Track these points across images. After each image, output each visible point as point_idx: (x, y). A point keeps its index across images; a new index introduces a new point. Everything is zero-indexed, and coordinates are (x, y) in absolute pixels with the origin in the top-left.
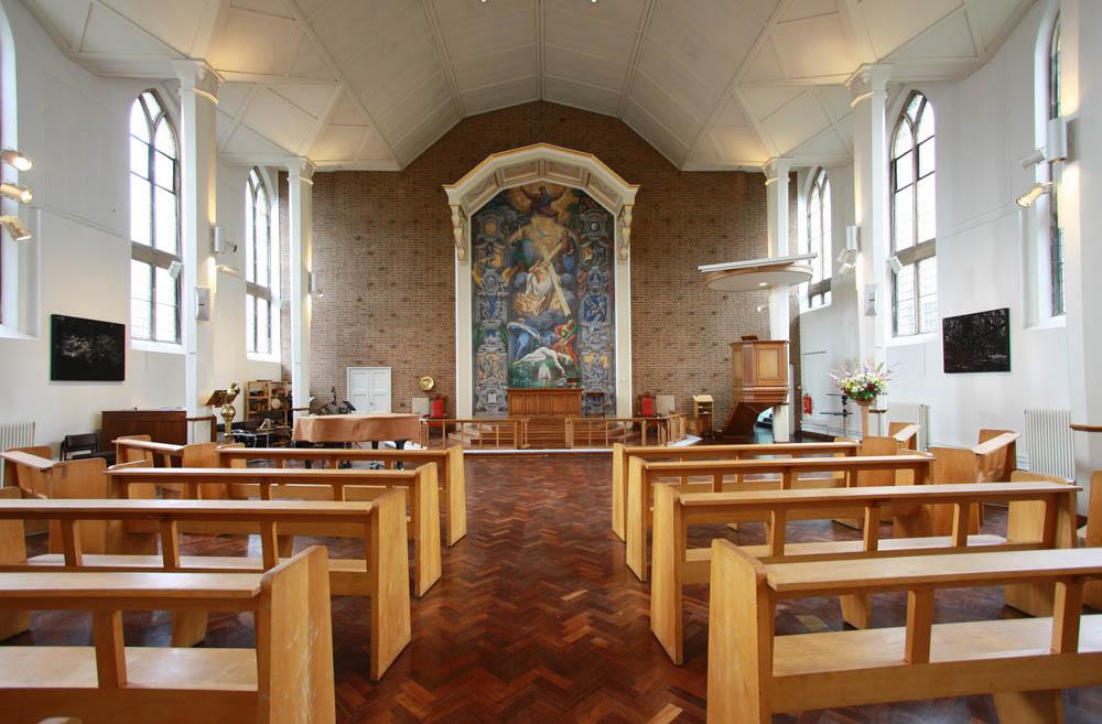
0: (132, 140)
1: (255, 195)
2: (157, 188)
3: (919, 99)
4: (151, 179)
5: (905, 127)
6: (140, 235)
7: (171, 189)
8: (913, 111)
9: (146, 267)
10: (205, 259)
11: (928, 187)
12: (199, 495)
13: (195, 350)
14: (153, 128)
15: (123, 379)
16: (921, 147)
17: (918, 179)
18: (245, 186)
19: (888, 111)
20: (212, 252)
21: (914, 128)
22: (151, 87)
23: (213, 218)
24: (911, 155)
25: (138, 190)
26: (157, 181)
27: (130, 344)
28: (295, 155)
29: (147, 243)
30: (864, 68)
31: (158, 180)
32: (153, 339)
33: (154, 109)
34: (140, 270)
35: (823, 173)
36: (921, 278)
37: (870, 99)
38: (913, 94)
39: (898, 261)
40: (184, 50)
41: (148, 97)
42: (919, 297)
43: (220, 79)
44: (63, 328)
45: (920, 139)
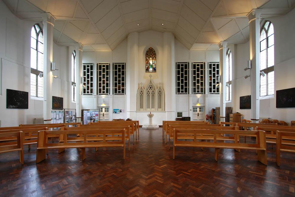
0: (32, 38)
1: (74, 57)
2: (39, 53)
3: (268, 23)
4: (37, 50)
5: (263, 31)
6: (33, 66)
7: (36, 49)
8: (266, 27)
9: (35, 76)
10: (49, 72)
11: (271, 50)
12: (191, 87)
13: (257, 100)
14: (38, 35)
15: (28, 108)
16: (269, 38)
17: (260, 52)
18: (72, 56)
19: (260, 23)
20: (51, 70)
21: (267, 32)
22: (37, 23)
23: (51, 60)
24: (265, 40)
25: (33, 53)
26: (39, 50)
27: (30, 98)
28: (77, 43)
29: (36, 69)
30: (253, 10)
31: (39, 49)
32: (37, 96)
33: (38, 30)
34: (33, 76)
35: (229, 50)
36: (268, 78)
37: (255, 20)
38: (266, 21)
39: (264, 73)
40: (44, 10)
41: (36, 26)
42: (268, 84)
43: (55, 19)
44: (10, 93)
45: (269, 35)
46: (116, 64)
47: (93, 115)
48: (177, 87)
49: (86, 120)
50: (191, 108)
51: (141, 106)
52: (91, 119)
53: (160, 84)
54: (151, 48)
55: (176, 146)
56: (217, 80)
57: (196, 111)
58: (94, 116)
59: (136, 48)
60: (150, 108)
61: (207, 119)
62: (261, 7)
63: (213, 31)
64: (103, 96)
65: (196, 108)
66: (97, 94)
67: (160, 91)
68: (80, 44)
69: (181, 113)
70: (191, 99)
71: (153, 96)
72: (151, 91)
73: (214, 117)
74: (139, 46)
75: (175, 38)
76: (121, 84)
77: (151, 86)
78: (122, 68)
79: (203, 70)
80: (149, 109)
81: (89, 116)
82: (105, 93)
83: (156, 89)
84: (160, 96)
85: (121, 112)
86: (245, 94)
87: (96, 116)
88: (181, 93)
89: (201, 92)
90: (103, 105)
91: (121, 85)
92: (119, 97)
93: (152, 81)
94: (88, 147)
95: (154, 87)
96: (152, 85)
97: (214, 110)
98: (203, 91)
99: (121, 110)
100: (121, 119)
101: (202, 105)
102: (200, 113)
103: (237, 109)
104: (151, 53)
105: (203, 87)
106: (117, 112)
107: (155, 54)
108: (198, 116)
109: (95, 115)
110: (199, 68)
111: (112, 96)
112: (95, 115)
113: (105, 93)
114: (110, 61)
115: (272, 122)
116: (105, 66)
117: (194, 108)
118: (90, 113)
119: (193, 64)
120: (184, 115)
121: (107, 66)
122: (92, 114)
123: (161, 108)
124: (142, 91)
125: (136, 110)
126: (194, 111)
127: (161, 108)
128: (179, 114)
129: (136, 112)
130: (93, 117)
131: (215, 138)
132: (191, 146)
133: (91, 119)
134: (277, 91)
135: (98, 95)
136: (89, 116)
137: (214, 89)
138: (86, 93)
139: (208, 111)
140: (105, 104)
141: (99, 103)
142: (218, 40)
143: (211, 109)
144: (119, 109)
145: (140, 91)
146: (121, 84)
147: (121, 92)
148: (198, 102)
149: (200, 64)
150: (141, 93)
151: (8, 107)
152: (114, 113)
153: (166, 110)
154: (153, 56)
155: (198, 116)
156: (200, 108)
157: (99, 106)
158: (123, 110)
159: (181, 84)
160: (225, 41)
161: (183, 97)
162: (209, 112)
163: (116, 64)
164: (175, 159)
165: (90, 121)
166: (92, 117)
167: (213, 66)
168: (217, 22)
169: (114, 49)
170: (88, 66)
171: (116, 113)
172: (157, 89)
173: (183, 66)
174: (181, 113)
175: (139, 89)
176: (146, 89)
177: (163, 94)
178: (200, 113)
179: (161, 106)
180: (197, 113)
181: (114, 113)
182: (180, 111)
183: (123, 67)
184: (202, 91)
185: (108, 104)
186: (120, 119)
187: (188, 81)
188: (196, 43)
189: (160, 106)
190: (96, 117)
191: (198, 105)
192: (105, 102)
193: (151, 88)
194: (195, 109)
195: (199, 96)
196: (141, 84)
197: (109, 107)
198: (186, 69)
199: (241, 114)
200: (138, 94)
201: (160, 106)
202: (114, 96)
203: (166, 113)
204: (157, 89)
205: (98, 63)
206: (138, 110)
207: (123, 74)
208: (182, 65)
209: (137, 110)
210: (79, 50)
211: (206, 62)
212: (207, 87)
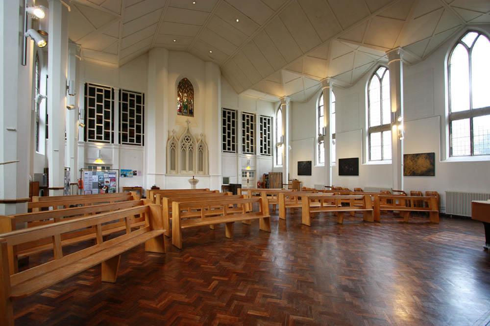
46: (224, 110)
47: (105, 180)
48: (142, 134)
49: (90, 187)
50: (240, 173)
51: (173, 167)
52: (101, 187)
53: (202, 135)
54: (185, 79)
55: (185, 229)
56: (269, 139)
57: (246, 176)
58: (107, 182)
59: (164, 74)
60: (192, 170)
61: (258, 187)
62: (334, 77)
63: (280, 83)
64: (99, 145)
65: (246, 173)
66: (85, 140)
67: (173, 144)
68: (78, 46)
69: (228, 178)
70: (240, 159)
71: (191, 152)
72: (188, 144)
73: (266, 184)
74: (169, 72)
75: (222, 74)
76: (135, 127)
77: (187, 137)
78: (105, 96)
79: (254, 123)
80: (191, 172)
81: (97, 181)
82: (103, 140)
83: (196, 142)
84: (173, 151)
85: (135, 174)
86: (304, 159)
87: (110, 181)
88: (128, 142)
89: (136, 142)
90: (99, 162)
91: (135, 129)
92: (130, 150)
93: (190, 130)
94: (332, 212)
95: (193, 139)
96: (189, 135)
97: (266, 176)
98: (253, 151)
99: (136, 171)
100: (139, 186)
101: (253, 169)
102: (249, 178)
103: (295, 176)
104: (185, 87)
105: (236, 144)
106: (128, 175)
107: (192, 90)
108: (248, 182)
109: (109, 180)
110: (249, 120)
111: (118, 147)
112: (109, 180)
113: (103, 140)
114: (116, 84)
115: (336, 189)
116: (104, 91)
117: (243, 173)
118: (99, 176)
119: (242, 113)
120: (232, 181)
121: (107, 94)
122: (104, 178)
123: (202, 170)
124: (175, 142)
125: (165, 173)
126: (243, 176)
127: (202, 170)
128: (226, 180)
129: (166, 176)
130: (105, 184)
131: (322, 205)
132: (73, 242)
133: (101, 187)
134: (339, 160)
135: (87, 142)
136: (97, 181)
137: (267, 149)
138: (227, 150)
139: (259, 177)
140: (102, 160)
141: (90, 156)
142: (281, 94)
143: (262, 175)
144: (131, 170)
145: (172, 142)
146: (135, 127)
147: (103, 138)
148: (248, 164)
149: (250, 115)
150: (173, 147)
151: (358, 175)
152: (123, 176)
153: (210, 174)
154: (188, 91)
155: (248, 182)
156: (250, 173)
157: (90, 162)
158: (140, 172)
159: (97, 123)
160: (288, 96)
161: (229, 156)
162: (260, 178)
163: (224, 110)
164: (185, 245)
165: (97, 189)
166: (103, 183)
167: (98, 91)
168: (287, 75)
169: (123, 66)
170: (248, 116)
171: (125, 176)
172: (198, 142)
173: (134, 97)
174: (228, 178)
175: (168, 140)
176: (180, 140)
177: (206, 151)
178: (249, 178)
179: (202, 167)
180: (246, 178)
181: (123, 176)
182: (226, 176)
183: (140, 99)
184: (252, 151)
185: (110, 160)
186: (136, 187)
187: (142, 125)
188: (253, 89)
189: (201, 168)
190: (112, 184)
191: (248, 168)
192: (102, 157)
193: (187, 139)
194: (244, 174)
195: (249, 156)
196: (174, 131)
197: (111, 165)
198: (234, 120)
199: (300, 181)
200: (168, 148)
201: (201, 168)
202: (123, 147)
203: (211, 178)
204: (198, 142)
205: (88, 82)
206: (168, 172)
207: (139, 110)
208: (229, 113)
209: (167, 173)
210: (76, 57)
211: (257, 115)
212: (258, 146)
